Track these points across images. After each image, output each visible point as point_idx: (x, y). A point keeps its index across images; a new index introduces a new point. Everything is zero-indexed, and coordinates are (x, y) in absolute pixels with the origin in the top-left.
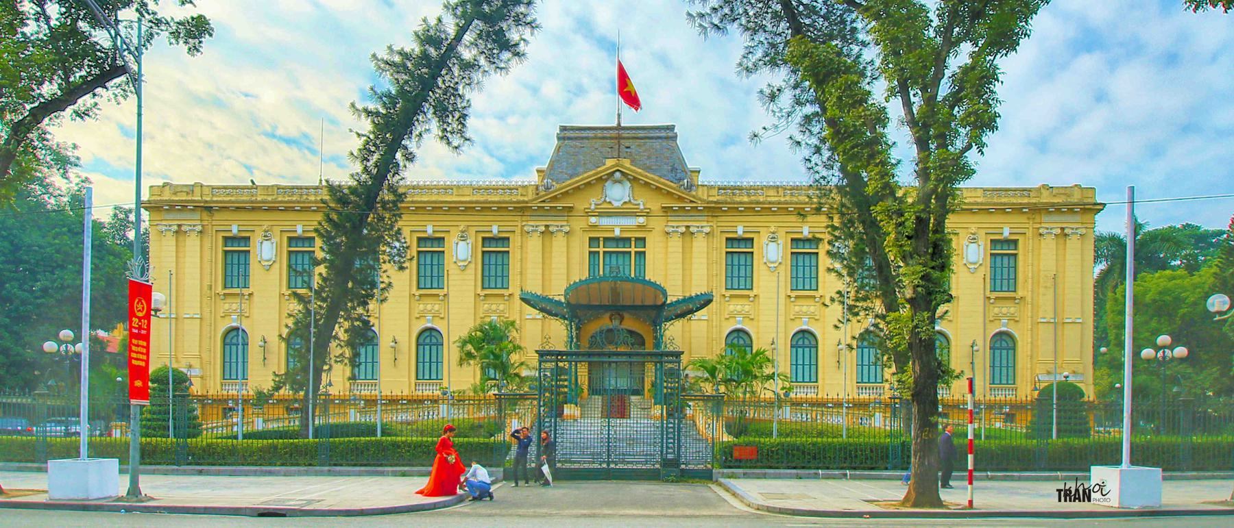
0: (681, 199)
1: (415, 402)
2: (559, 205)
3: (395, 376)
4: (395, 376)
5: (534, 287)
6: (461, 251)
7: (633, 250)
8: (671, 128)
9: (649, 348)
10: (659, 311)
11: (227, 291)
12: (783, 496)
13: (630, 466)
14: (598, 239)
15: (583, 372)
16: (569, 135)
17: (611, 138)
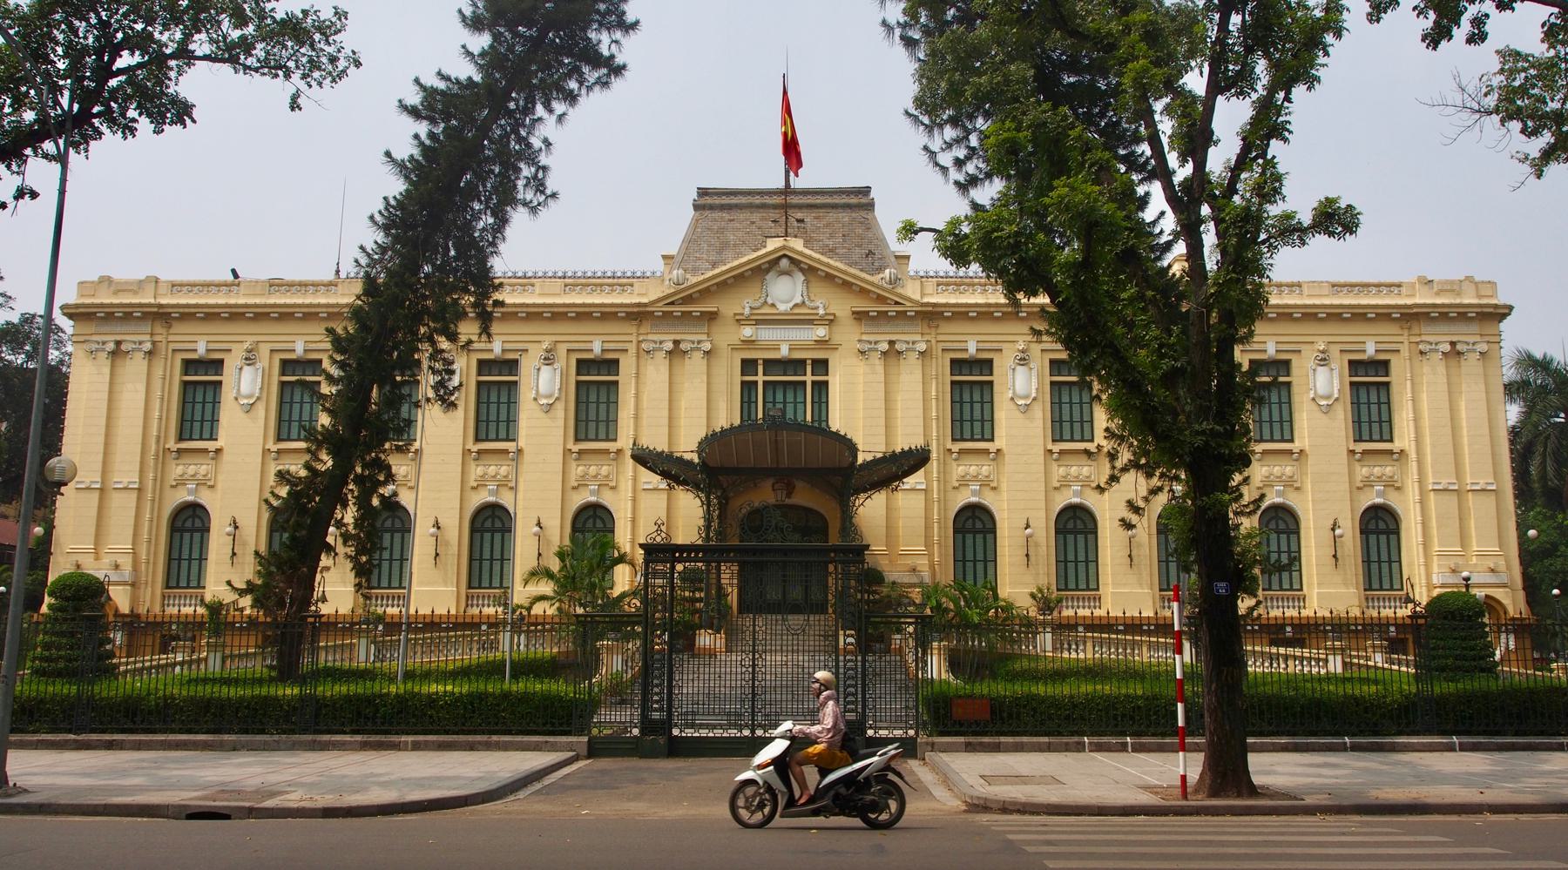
0: (881, 299)
1: (463, 626)
2: (696, 309)
3: (432, 589)
4: (432, 589)
5: (656, 441)
6: (543, 385)
7: (809, 378)
8: (866, 191)
9: (834, 539)
10: (849, 475)
11: (184, 445)
12: (124, 773)
13: (704, 733)
14: (755, 361)
15: (729, 577)
16: (710, 201)
17: (775, 207)
